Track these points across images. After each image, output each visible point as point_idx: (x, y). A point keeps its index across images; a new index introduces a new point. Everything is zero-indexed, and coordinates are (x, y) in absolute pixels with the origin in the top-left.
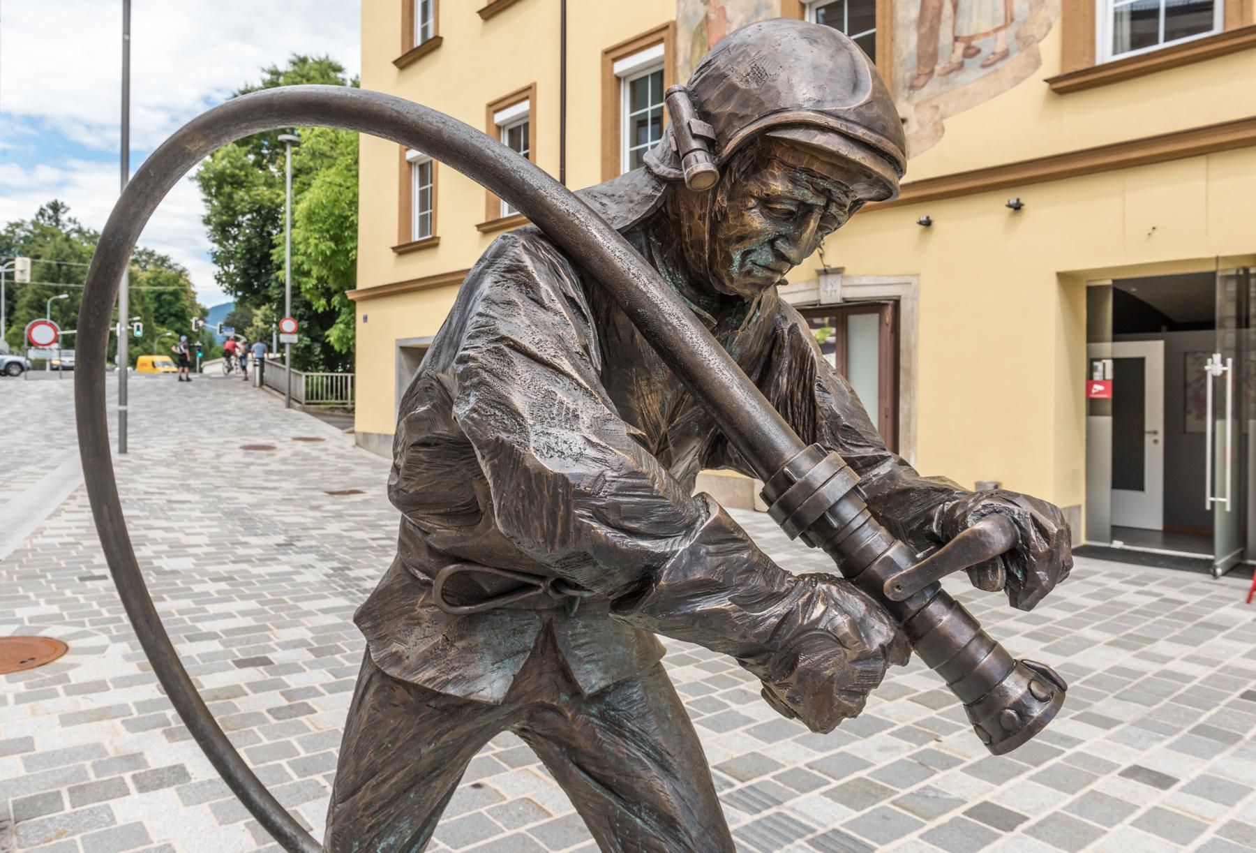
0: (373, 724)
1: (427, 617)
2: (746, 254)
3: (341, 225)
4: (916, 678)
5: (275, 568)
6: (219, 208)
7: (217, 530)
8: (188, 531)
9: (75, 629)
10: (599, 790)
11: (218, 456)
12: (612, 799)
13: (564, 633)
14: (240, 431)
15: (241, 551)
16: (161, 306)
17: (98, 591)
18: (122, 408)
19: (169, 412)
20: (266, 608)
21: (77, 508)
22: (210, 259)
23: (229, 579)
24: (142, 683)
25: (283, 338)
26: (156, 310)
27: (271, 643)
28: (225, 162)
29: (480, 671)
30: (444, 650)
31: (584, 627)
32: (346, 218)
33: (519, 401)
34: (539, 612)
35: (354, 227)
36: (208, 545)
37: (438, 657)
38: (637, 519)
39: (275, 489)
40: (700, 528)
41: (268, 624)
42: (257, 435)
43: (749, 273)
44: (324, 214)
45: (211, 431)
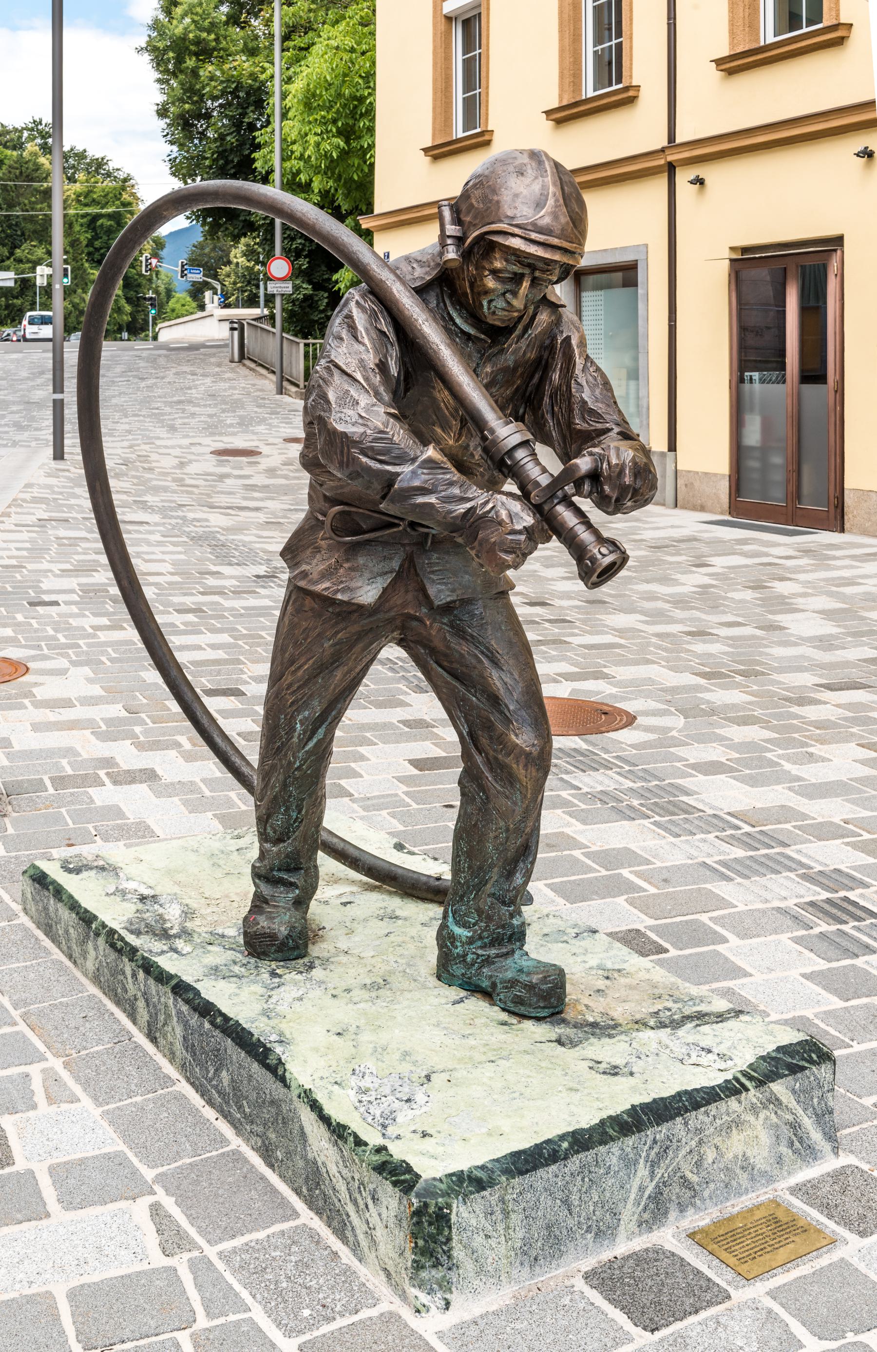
0: (293, 626)
1: (325, 547)
2: (490, 302)
3: (353, 114)
4: (553, 548)
5: (252, 602)
6: (179, 92)
7: (183, 557)
8: (146, 557)
9: (33, 652)
10: (449, 679)
11: (182, 465)
12: (457, 685)
13: (422, 562)
14: (212, 429)
15: (211, 582)
16: (96, 237)
17: (52, 616)
18: (58, 396)
19: (114, 401)
20: (240, 642)
21: (13, 528)
22: (166, 168)
23: (197, 610)
24: (107, 703)
25: (272, 288)
26: (90, 243)
27: (244, 676)
28: (188, 20)
29: (359, 584)
30: (336, 569)
31: (438, 558)
32: (361, 100)
33: (331, 396)
34: (403, 545)
35: (370, 113)
36: (172, 574)
37: (331, 574)
38: (384, 455)
39: (257, 509)
40: (420, 459)
41: (241, 658)
42: (234, 434)
43: (494, 313)
44: (326, 96)
45: (172, 428)
